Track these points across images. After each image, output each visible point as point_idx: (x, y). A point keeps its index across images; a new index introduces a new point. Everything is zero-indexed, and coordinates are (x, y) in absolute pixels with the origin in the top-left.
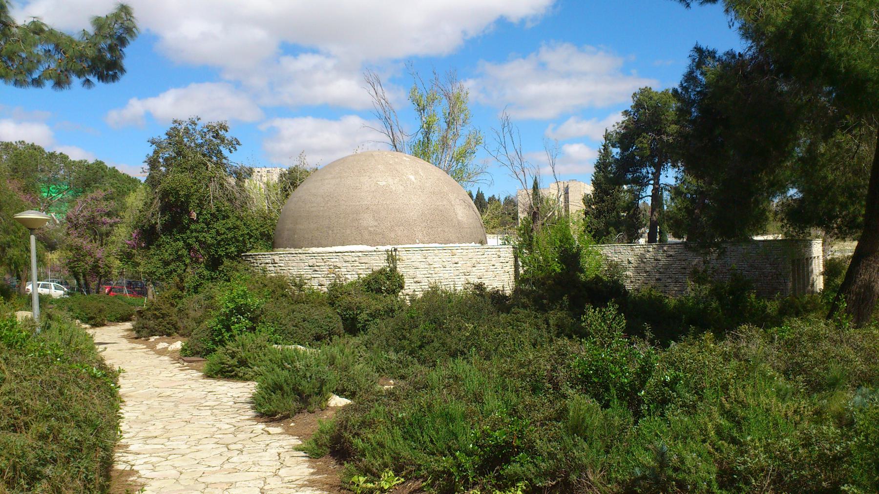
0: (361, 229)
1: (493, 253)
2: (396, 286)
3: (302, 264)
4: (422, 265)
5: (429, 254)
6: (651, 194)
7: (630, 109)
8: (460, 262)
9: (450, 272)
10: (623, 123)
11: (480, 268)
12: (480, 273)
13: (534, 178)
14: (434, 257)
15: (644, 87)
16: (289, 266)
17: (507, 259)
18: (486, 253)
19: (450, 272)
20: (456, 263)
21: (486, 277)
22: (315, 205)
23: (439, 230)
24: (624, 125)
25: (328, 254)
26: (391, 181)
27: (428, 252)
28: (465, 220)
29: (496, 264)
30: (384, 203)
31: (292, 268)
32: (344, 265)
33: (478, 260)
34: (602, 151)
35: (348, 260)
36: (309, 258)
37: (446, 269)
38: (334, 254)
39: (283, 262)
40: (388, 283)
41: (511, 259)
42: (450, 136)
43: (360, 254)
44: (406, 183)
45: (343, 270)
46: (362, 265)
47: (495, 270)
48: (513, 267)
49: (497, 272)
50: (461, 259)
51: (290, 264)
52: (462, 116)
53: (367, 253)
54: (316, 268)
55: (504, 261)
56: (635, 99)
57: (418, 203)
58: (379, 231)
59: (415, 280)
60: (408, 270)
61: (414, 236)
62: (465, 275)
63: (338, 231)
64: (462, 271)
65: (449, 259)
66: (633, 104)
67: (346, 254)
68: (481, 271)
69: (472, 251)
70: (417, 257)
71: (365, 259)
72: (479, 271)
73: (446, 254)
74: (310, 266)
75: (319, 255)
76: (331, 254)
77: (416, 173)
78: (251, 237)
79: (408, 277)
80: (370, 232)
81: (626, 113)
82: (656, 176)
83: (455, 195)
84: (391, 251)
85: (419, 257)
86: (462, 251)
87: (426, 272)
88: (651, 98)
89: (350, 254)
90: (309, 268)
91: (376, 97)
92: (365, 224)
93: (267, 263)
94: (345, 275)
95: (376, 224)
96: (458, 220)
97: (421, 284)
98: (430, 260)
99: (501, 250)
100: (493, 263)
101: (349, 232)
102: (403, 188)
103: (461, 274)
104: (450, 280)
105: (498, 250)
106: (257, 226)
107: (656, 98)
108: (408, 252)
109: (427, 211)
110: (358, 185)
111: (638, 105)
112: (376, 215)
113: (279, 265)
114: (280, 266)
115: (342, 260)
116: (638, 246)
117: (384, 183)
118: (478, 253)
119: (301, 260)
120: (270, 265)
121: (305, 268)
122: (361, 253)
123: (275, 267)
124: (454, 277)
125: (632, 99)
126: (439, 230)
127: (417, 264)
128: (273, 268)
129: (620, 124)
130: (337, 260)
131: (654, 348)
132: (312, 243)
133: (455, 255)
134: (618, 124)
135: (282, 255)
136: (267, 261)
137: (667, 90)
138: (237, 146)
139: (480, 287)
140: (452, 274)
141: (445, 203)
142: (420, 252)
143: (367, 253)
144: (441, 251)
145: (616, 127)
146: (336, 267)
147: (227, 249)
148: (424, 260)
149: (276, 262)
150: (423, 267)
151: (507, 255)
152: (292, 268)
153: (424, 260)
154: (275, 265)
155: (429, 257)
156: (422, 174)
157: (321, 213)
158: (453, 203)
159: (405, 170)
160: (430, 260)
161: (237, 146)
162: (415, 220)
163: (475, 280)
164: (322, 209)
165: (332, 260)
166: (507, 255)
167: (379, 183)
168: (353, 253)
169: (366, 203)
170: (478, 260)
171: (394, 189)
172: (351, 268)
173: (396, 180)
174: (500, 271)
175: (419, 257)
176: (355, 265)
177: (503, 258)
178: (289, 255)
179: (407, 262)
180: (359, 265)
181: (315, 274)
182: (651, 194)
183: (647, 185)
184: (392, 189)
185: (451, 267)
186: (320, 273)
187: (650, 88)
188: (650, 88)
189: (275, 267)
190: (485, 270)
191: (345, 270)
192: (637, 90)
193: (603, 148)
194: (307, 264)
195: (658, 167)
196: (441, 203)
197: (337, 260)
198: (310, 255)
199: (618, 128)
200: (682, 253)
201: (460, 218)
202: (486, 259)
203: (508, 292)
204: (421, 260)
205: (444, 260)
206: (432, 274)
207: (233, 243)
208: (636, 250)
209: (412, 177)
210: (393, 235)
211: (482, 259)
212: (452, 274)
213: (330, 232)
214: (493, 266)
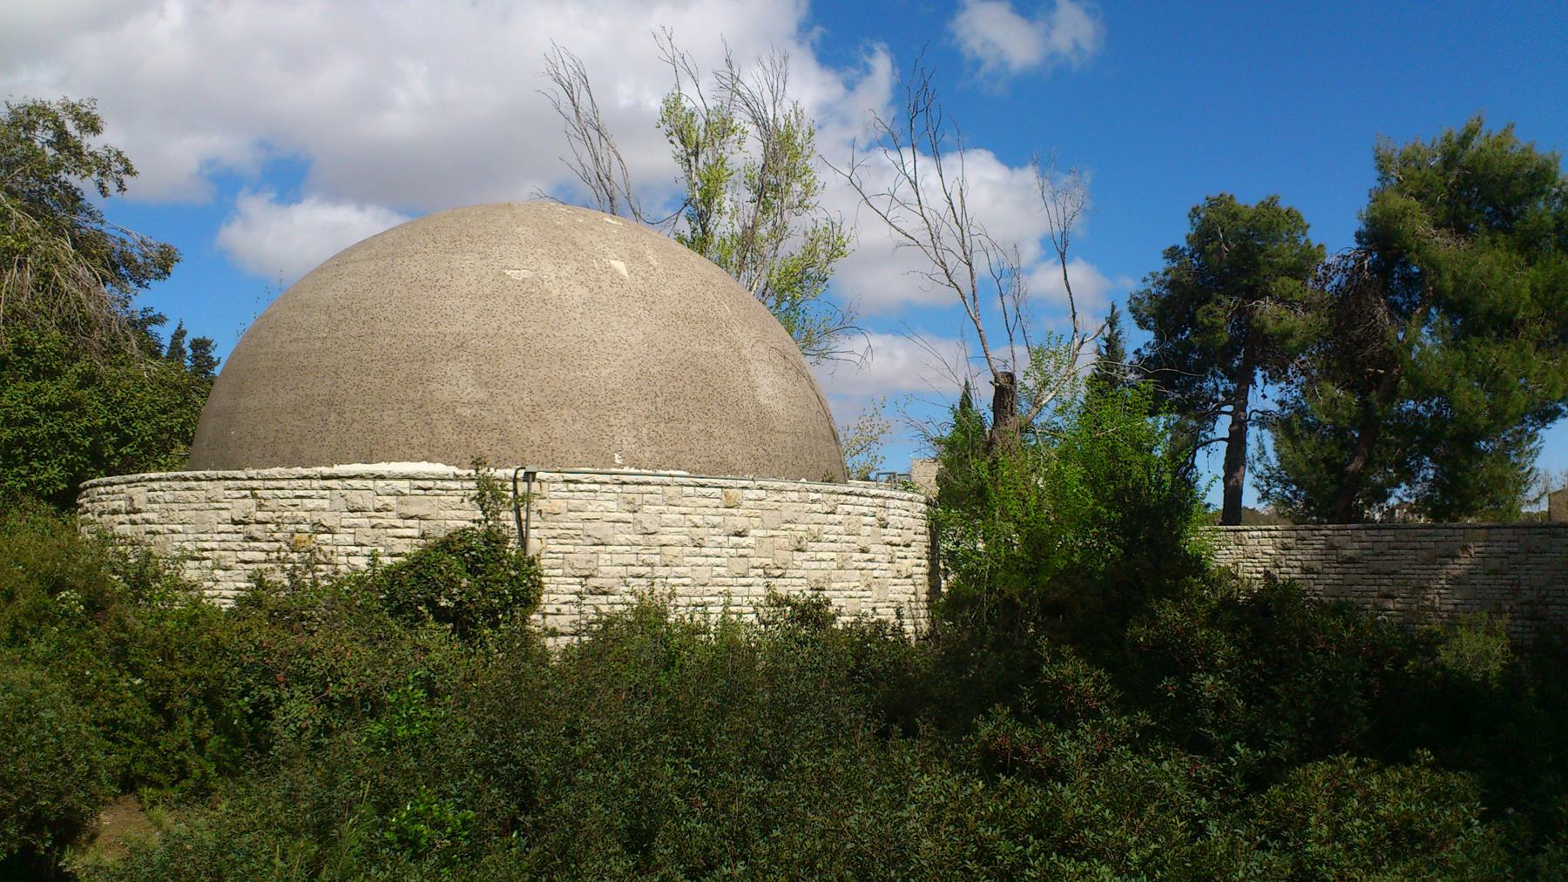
0: (430, 408)
1: (865, 510)
2: (501, 596)
3: (212, 515)
4: (623, 535)
5: (647, 497)
6: (1227, 435)
7: (1183, 244)
8: (753, 532)
9: (718, 561)
10: (1166, 274)
11: (820, 555)
12: (819, 574)
13: (963, 384)
14: (664, 508)
15: (1218, 195)
16: (172, 521)
17: (909, 536)
18: (839, 510)
19: (718, 561)
20: (738, 534)
21: (837, 586)
22: (302, 334)
23: (694, 428)
24: (1168, 278)
25: (294, 483)
26: (548, 269)
27: (642, 488)
28: (779, 406)
29: (873, 548)
30: (519, 331)
31: (180, 528)
32: (345, 522)
33: (815, 528)
34: (1104, 351)
35: (360, 503)
36: (236, 494)
37: (705, 551)
38: (315, 484)
39: (156, 506)
40: (465, 583)
41: (919, 537)
42: (763, 231)
43: (404, 485)
44: (598, 280)
45: (344, 537)
46: (410, 523)
47: (871, 565)
48: (925, 562)
49: (876, 573)
50: (757, 522)
51: (177, 516)
52: (797, 187)
53: (430, 484)
54: (255, 530)
55: (897, 540)
56: (1196, 220)
57: (632, 340)
58: (491, 418)
59: (592, 582)
60: (570, 548)
61: (606, 442)
62: (767, 575)
63: (357, 416)
64: (756, 562)
65: (717, 520)
66: (1193, 233)
67: (356, 483)
68: (824, 565)
69: (795, 496)
70: (606, 504)
71: (420, 503)
72: (815, 565)
73: (705, 501)
74: (235, 522)
75: (268, 484)
76: (307, 483)
77: (635, 257)
78: (125, 440)
79: (569, 570)
80: (461, 422)
81: (1173, 253)
82: (1238, 399)
83: (753, 333)
84: (515, 480)
85: (612, 505)
86: (762, 493)
87: (632, 559)
88: (1234, 217)
89: (370, 484)
90: (232, 528)
91: (575, 122)
92: (445, 394)
93: (115, 512)
94: (348, 555)
95: (482, 395)
96: (758, 405)
97: (612, 599)
98: (647, 517)
99: (891, 503)
100: (862, 542)
101: (389, 420)
102: (584, 292)
103: (753, 572)
104: (716, 590)
105: (878, 501)
106: (148, 408)
107: (1246, 216)
108: (572, 486)
109: (659, 368)
110: (441, 275)
111: (1204, 236)
112: (486, 367)
113: (145, 515)
114: (147, 522)
115: (340, 503)
116: (1255, 533)
117: (525, 274)
118: (816, 507)
119: (209, 500)
120: (121, 518)
121: (221, 528)
122: (406, 483)
123: (133, 523)
124: (729, 581)
125: (1189, 220)
126: (694, 428)
127: (602, 530)
128: (127, 529)
129: (1160, 277)
130: (325, 504)
131: (1216, 781)
132: (275, 454)
133: (737, 506)
134: (1154, 275)
135: (156, 485)
136: (115, 505)
137: (1272, 199)
138: (126, 178)
139: (812, 614)
140: (721, 570)
141: (718, 348)
142: (616, 488)
143: (430, 484)
144: (688, 490)
145: (1151, 282)
146: (319, 528)
147: (34, 470)
148: (629, 516)
149: (137, 506)
150: (621, 538)
151: (909, 522)
152: (180, 528)
153: (629, 516)
154: (133, 517)
155: (646, 507)
156: (654, 263)
157: (313, 359)
158: (744, 352)
159: (601, 246)
160: (647, 517)
161: (126, 178)
162: (615, 392)
163: (794, 587)
164: (318, 344)
165: (309, 503)
166: (909, 522)
167: (508, 273)
168: (381, 483)
169: (457, 328)
170: (815, 528)
171: (555, 292)
172: (370, 532)
173: (569, 269)
174: (882, 570)
175: (612, 505)
176: (385, 523)
177: (896, 531)
178: (175, 484)
179: (569, 521)
180: (399, 523)
181: (253, 550)
182: (1227, 435)
183: (1214, 416)
184: (548, 292)
185: (720, 546)
186: (264, 546)
187: (1231, 197)
188: (1231, 197)
189: (133, 523)
190: (834, 565)
191: (350, 539)
192: (1200, 202)
193: (1105, 343)
194: (225, 514)
195: (1244, 379)
196: (704, 349)
197: (325, 504)
198: (239, 483)
199: (1154, 285)
200: (1382, 553)
201: (763, 401)
202: (840, 529)
203: (915, 626)
204: (617, 516)
205: (697, 519)
206: (652, 565)
207: (57, 452)
208: (1250, 542)
209: (620, 267)
210: (535, 435)
211: (827, 528)
212: (721, 570)
213: (333, 417)
214: (863, 551)
